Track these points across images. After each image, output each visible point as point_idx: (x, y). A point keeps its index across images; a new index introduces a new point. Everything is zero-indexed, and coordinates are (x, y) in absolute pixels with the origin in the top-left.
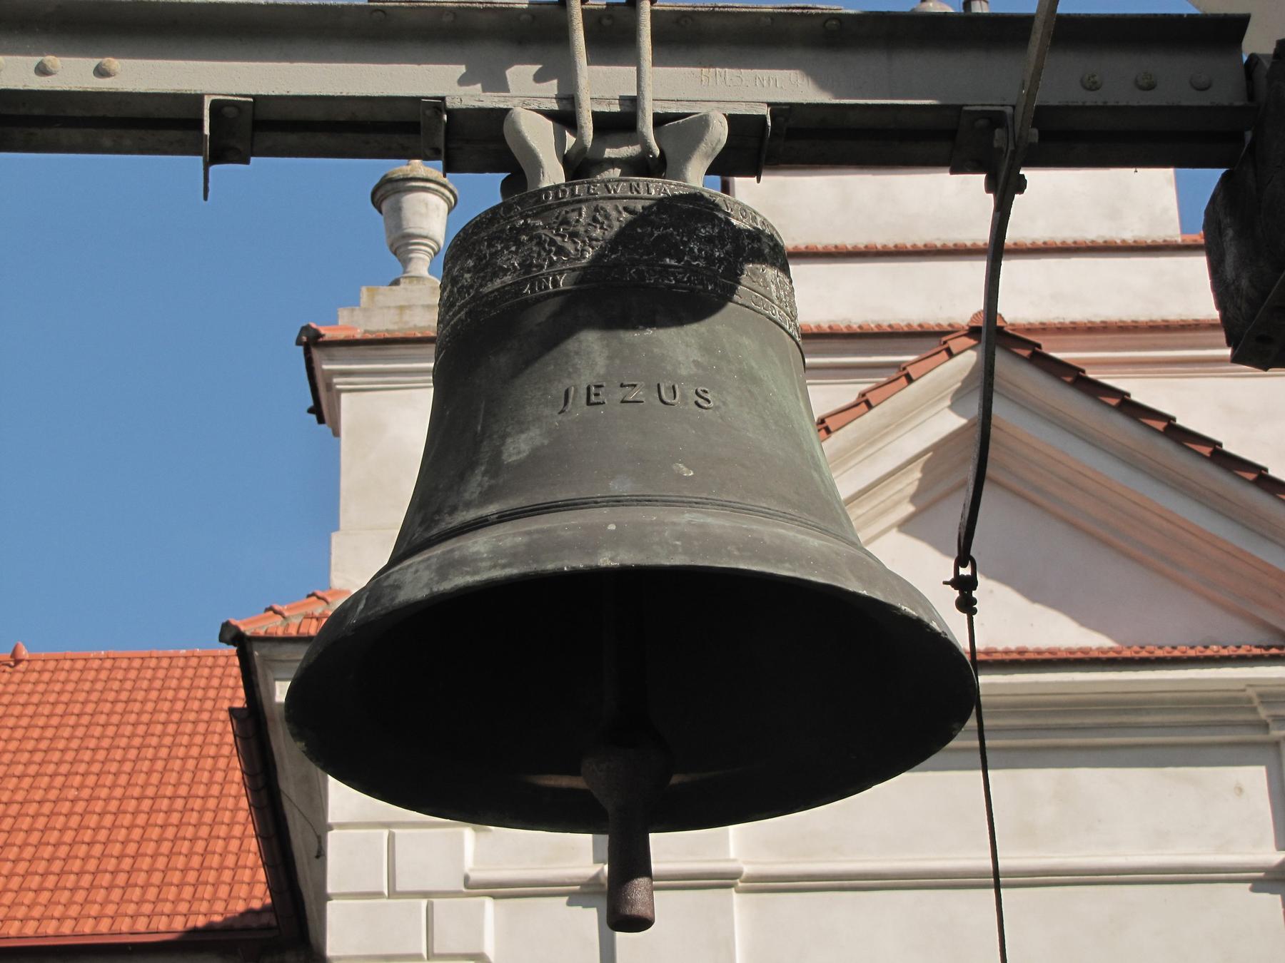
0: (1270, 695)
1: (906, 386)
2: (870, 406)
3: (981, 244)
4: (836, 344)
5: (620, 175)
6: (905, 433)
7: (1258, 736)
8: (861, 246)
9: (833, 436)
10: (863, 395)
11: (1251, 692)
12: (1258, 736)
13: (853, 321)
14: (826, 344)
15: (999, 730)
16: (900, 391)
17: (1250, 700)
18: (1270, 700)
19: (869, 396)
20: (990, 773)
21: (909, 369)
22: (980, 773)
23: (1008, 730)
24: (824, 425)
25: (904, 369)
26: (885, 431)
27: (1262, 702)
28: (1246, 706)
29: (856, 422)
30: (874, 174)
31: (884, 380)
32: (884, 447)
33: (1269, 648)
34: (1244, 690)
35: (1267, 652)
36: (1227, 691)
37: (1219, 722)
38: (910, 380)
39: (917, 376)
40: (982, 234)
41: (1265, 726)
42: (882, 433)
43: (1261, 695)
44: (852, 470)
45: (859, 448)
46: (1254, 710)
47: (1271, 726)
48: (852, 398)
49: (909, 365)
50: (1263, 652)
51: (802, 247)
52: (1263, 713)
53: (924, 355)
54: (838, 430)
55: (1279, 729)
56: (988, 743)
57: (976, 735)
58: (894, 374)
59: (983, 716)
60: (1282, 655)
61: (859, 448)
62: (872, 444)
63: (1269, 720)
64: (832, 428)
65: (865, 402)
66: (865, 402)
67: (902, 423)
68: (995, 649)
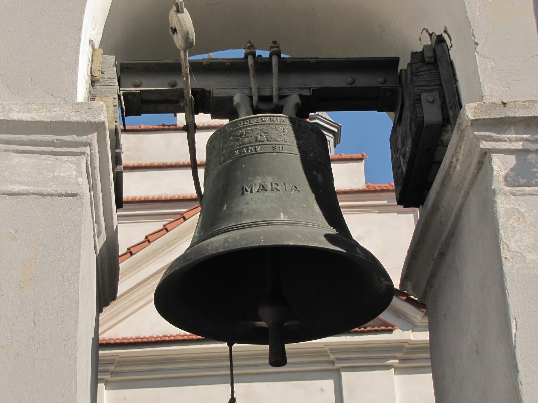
0: (335, 349)
1: (184, 222)
2: (167, 231)
3: (186, 163)
4: (159, 205)
5: (230, 121)
6: (185, 241)
7: (330, 367)
8: (174, 163)
9: (152, 244)
10: (164, 226)
11: (326, 348)
12: (330, 367)
13: (169, 195)
14: (155, 205)
15: (225, 367)
16: (181, 224)
17: (326, 352)
18: (334, 351)
19: (167, 226)
20: (235, 385)
21: (185, 215)
22: (229, 385)
23: (376, 358)
24: (147, 239)
25: (182, 214)
26: (175, 241)
27: (331, 352)
28: (325, 354)
29: (161, 237)
30: (180, 133)
31: (173, 220)
32: (175, 248)
33: (374, 327)
34: (324, 347)
35: (359, 330)
36: (317, 348)
37: (314, 361)
38: (185, 219)
39: (188, 218)
40: (187, 159)
41: (333, 363)
42: (173, 242)
43: (330, 350)
44: (161, 258)
45: (164, 248)
46: (328, 356)
47: (335, 362)
48: (161, 227)
49: (184, 213)
50: (372, 328)
51: (149, 164)
52: (332, 357)
53: (191, 209)
54: (153, 241)
55: (338, 364)
56: (234, 372)
57: (229, 368)
58: (179, 216)
59: (233, 360)
60: (366, 331)
61: (164, 248)
62: (170, 246)
63: (334, 360)
64: (151, 240)
65: (166, 229)
66: (166, 229)
67: (183, 237)
68: (167, 335)
